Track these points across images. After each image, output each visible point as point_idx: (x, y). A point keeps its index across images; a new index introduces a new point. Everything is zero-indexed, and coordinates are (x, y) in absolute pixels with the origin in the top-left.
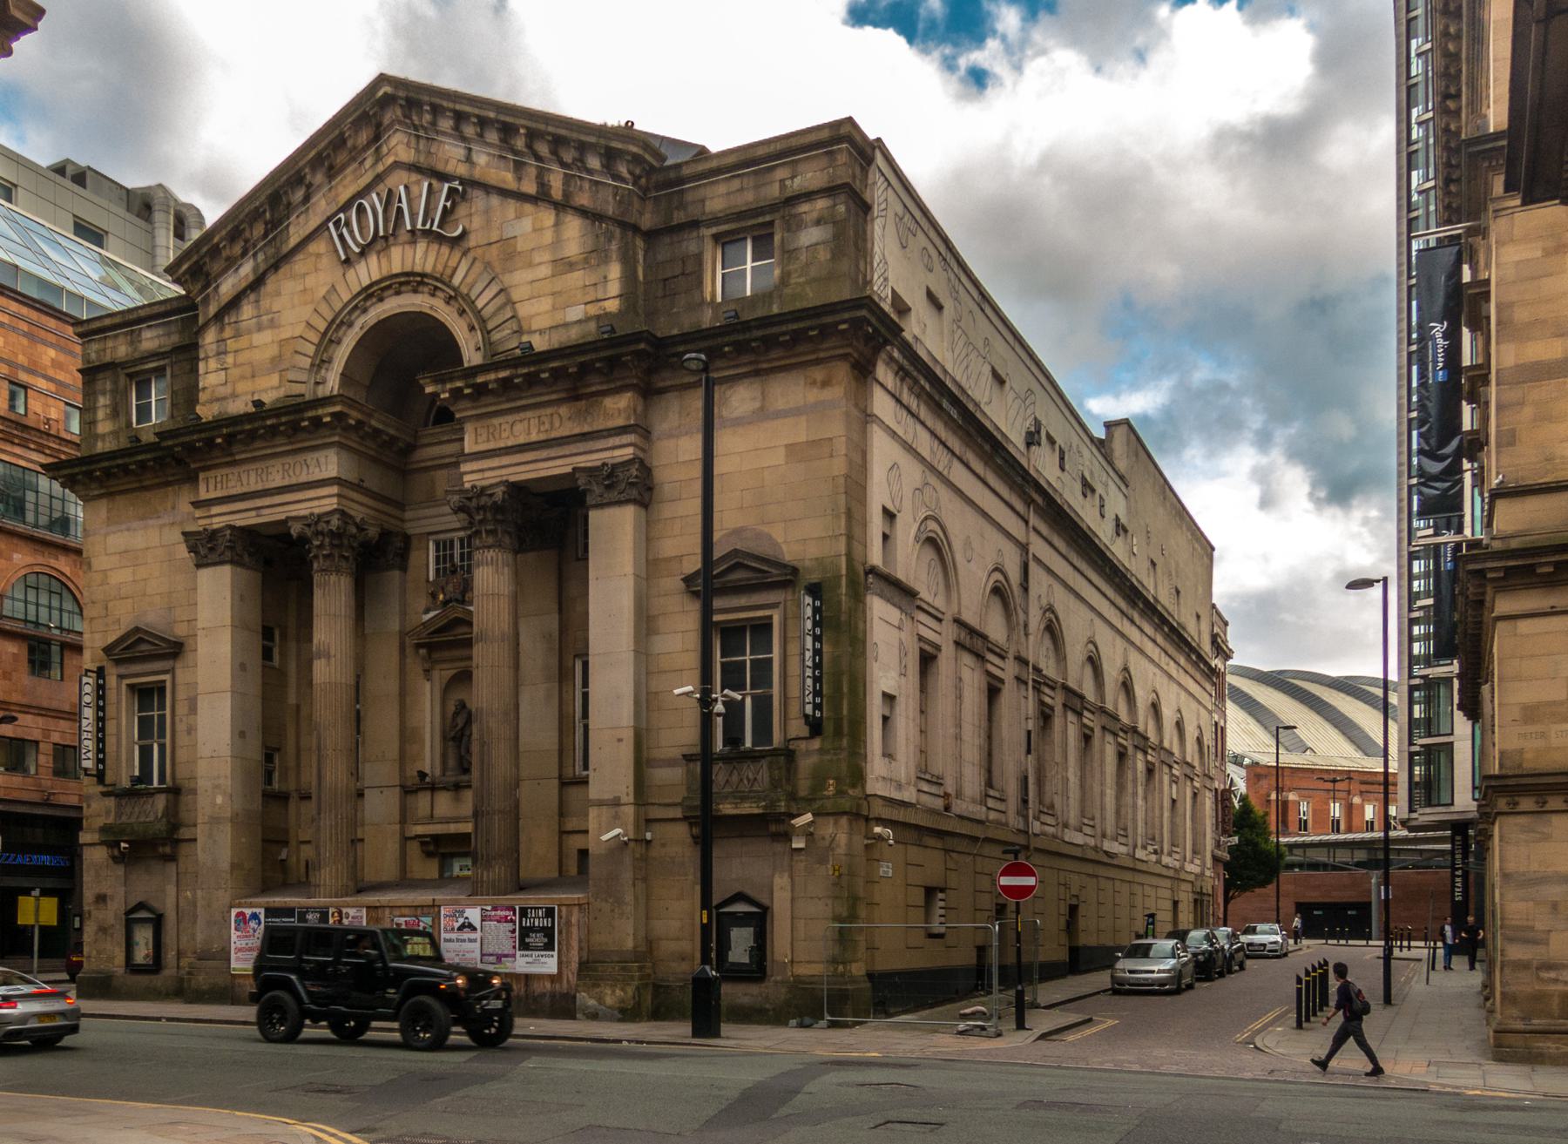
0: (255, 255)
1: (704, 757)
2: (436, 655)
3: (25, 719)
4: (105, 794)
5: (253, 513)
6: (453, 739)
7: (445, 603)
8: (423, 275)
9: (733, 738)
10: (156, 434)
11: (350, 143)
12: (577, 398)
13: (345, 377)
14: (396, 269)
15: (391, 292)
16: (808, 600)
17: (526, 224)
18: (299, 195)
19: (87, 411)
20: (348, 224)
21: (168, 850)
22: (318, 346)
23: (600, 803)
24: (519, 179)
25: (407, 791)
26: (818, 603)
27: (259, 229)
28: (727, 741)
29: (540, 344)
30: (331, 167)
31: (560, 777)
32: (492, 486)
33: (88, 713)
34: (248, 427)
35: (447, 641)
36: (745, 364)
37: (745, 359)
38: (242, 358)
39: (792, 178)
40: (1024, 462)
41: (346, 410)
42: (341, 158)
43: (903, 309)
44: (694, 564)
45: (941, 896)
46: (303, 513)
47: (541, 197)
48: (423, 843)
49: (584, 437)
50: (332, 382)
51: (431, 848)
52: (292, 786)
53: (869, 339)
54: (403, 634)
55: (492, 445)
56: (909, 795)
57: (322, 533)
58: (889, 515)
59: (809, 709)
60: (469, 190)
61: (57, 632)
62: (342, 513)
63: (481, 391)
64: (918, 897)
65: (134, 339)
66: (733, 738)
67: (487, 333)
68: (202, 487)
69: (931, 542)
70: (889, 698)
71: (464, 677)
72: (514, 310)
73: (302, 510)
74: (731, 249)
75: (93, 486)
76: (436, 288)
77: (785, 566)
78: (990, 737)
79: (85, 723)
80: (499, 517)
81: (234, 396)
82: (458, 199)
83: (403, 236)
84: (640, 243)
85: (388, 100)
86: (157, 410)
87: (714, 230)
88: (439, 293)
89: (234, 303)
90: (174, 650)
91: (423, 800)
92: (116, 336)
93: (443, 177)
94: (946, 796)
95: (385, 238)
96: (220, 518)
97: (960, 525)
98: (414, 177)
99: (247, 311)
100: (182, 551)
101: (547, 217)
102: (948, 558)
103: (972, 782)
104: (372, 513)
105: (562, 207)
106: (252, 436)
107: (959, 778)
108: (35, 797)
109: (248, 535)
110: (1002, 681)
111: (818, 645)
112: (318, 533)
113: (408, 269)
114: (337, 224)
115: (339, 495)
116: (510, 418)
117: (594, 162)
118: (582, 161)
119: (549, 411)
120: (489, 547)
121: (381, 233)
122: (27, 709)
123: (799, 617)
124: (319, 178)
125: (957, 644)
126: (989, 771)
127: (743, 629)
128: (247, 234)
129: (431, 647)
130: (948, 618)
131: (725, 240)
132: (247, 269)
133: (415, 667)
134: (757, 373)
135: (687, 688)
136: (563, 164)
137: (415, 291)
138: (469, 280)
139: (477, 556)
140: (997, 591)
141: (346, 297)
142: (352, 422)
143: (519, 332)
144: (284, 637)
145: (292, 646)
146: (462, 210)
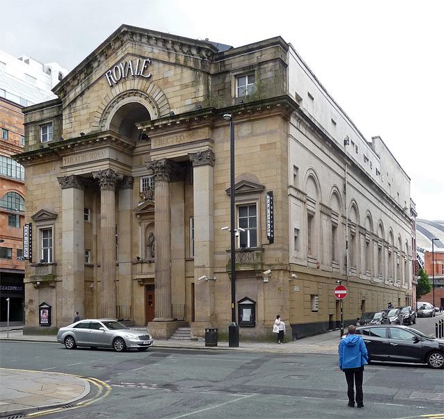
4: (32, 266)
7: (146, 200)
9: (243, 245)
11: (112, 47)
12: (190, 130)
16: (268, 197)
21: (53, 284)
23: (198, 267)
28: (241, 246)
32: (161, 160)
34: (79, 142)
35: (146, 213)
38: (77, 119)
42: (110, 52)
43: (300, 99)
44: (228, 186)
45: (316, 297)
50: (107, 126)
52: (94, 263)
56: (305, 263)
58: (296, 168)
63: (157, 128)
69: (311, 177)
70: (297, 230)
71: (152, 225)
73: (97, 169)
83: (130, 77)
84: (210, 78)
85: (125, 33)
86: (49, 137)
87: (235, 74)
89: (74, 100)
90: (54, 217)
91: (139, 266)
93: (144, 58)
96: (70, 173)
97: (322, 172)
98: (134, 58)
99: (79, 103)
101: (179, 70)
103: (327, 258)
105: (185, 66)
106: (80, 145)
109: (79, 177)
114: (108, 74)
117: (194, 52)
119: (179, 135)
122: (8, 237)
124: (102, 59)
126: (333, 255)
129: (140, 214)
132: (79, 90)
134: (250, 121)
136: (184, 53)
145: (94, 215)
146: (150, 68)
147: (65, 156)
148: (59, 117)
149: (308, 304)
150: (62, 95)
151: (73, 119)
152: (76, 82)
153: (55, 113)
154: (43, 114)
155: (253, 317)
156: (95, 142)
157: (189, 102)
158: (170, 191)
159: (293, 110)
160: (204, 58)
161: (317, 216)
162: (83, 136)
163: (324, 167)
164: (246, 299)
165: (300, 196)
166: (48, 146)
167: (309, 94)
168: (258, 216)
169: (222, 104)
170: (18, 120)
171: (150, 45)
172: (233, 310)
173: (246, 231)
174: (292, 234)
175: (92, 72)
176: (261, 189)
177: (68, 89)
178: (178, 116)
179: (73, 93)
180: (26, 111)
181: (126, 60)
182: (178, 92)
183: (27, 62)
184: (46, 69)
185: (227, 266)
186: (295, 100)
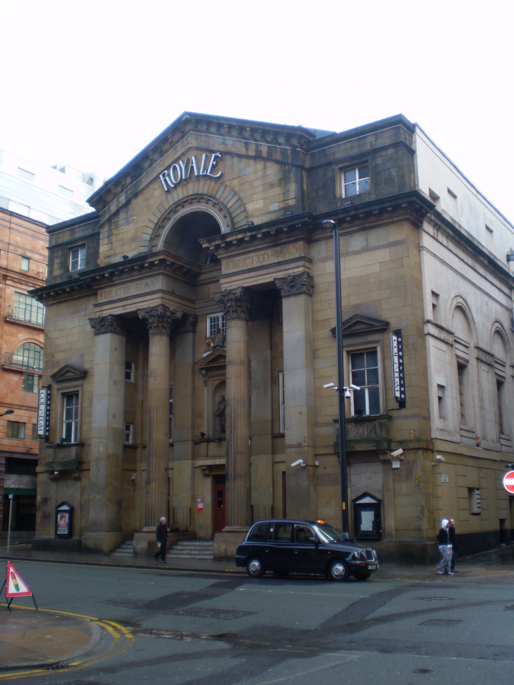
0: (127, 192)
1: (342, 420)
2: (210, 373)
3: (21, 412)
4: (49, 447)
5: (121, 308)
6: (218, 416)
7: (214, 347)
8: (202, 195)
9: (360, 409)
10: (78, 274)
11: (170, 141)
12: (277, 245)
13: (166, 242)
14: (191, 193)
15: (188, 203)
16: (395, 338)
17: (250, 170)
18: (147, 164)
19: (51, 265)
20: (169, 175)
21: (77, 475)
22: (154, 230)
23: (291, 446)
24: (247, 150)
25: (196, 443)
26: (400, 340)
27: (129, 180)
28: (356, 412)
29: (257, 221)
30: (161, 151)
31: (272, 434)
32: (234, 289)
33: (43, 407)
34: (121, 268)
35: (215, 366)
36: (358, 225)
37: (357, 222)
39: (376, 141)
40: (506, 269)
41: (165, 258)
42: (167, 146)
43: (435, 198)
44: (334, 324)
45: (477, 492)
46: (145, 307)
47: (258, 157)
48: (203, 470)
49: (279, 264)
50: (160, 245)
51: (207, 472)
52: (139, 441)
53: (417, 211)
54: (194, 363)
55: (235, 270)
56: (456, 438)
57: (153, 316)
58: (435, 295)
59: (398, 394)
60: (224, 156)
61: (37, 370)
62: (163, 305)
63: (229, 244)
64: (465, 492)
65: (73, 231)
66: (360, 409)
67: (232, 219)
68: (99, 297)
69: (459, 308)
70: (441, 387)
71: (223, 384)
72: (245, 207)
73: (144, 305)
74: (349, 174)
75: (50, 299)
76: (208, 200)
77: (382, 322)
78: (500, 408)
79: (40, 412)
80: (239, 304)
81: (115, 255)
82: (219, 160)
84: (304, 173)
86: (79, 262)
87: (340, 166)
88: (211, 203)
89: (117, 213)
90: (84, 375)
91: (203, 447)
92: (64, 232)
94: (477, 438)
95: (186, 180)
97: (475, 301)
98: (199, 152)
99: (122, 216)
100: (89, 328)
101: (260, 165)
102: (469, 315)
103: (492, 431)
104: (176, 305)
105: (269, 158)
106: (122, 272)
107: (484, 428)
108: (23, 450)
109: (119, 318)
110: (504, 378)
111: (401, 361)
112: (152, 316)
113: (196, 192)
114: (164, 175)
115: (162, 298)
116: (243, 257)
117: (281, 140)
118: (276, 139)
120: (234, 319)
121: (184, 178)
122: (20, 407)
123: (390, 346)
124: (156, 156)
125: (478, 359)
126: (501, 425)
127: (362, 354)
128: (123, 183)
129: (208, 370)
130: (472, 346)
131: (346, 169)
132: (122, 199)
133: (200, 381)
134: (364, 229)
135: (331, 384)
136: (267, 142)
137: (199, 202)
138: (224, 195)
139: (229, 323)
140: (498, 332)
141: (167, 207)
142: (169, 263)
143: (247, 217)
144: (136, 367)
146: (221, 165)
147: (101, 288)
148: (95, 237)
149: (464, 504)
150: (100, 206)
151: (114, 238)
152: (119, 189)
153: (90, 232)
154: (74, 233)
155: (377, 523)
156: (142, 267)
157: (275, 207)
158: (250, 333)
159: (427, 212)
160: (295, 147)
161: (473, 367)
162: (127, 261)
163: (478, 292)
164: (365, 495)
165: (443, 335)
166: (78, 276)
167: (449, 191)
168: (380, 366)
169: (322, 208)
170: (42, 243)
171: (221, 135)
172: (345, 513)
173: (362, 391)
174: (434, 393)
175: (141, 174)
176: (383, 327)
177: (109, 198)
178: (259, 227)
179: (115, 204)
180: (52, 230)
181: (187, 156)
182: (259, 196)
183: (63, 170)
184: (87, 179)
185: (336, 445)
186: (429, 199)
